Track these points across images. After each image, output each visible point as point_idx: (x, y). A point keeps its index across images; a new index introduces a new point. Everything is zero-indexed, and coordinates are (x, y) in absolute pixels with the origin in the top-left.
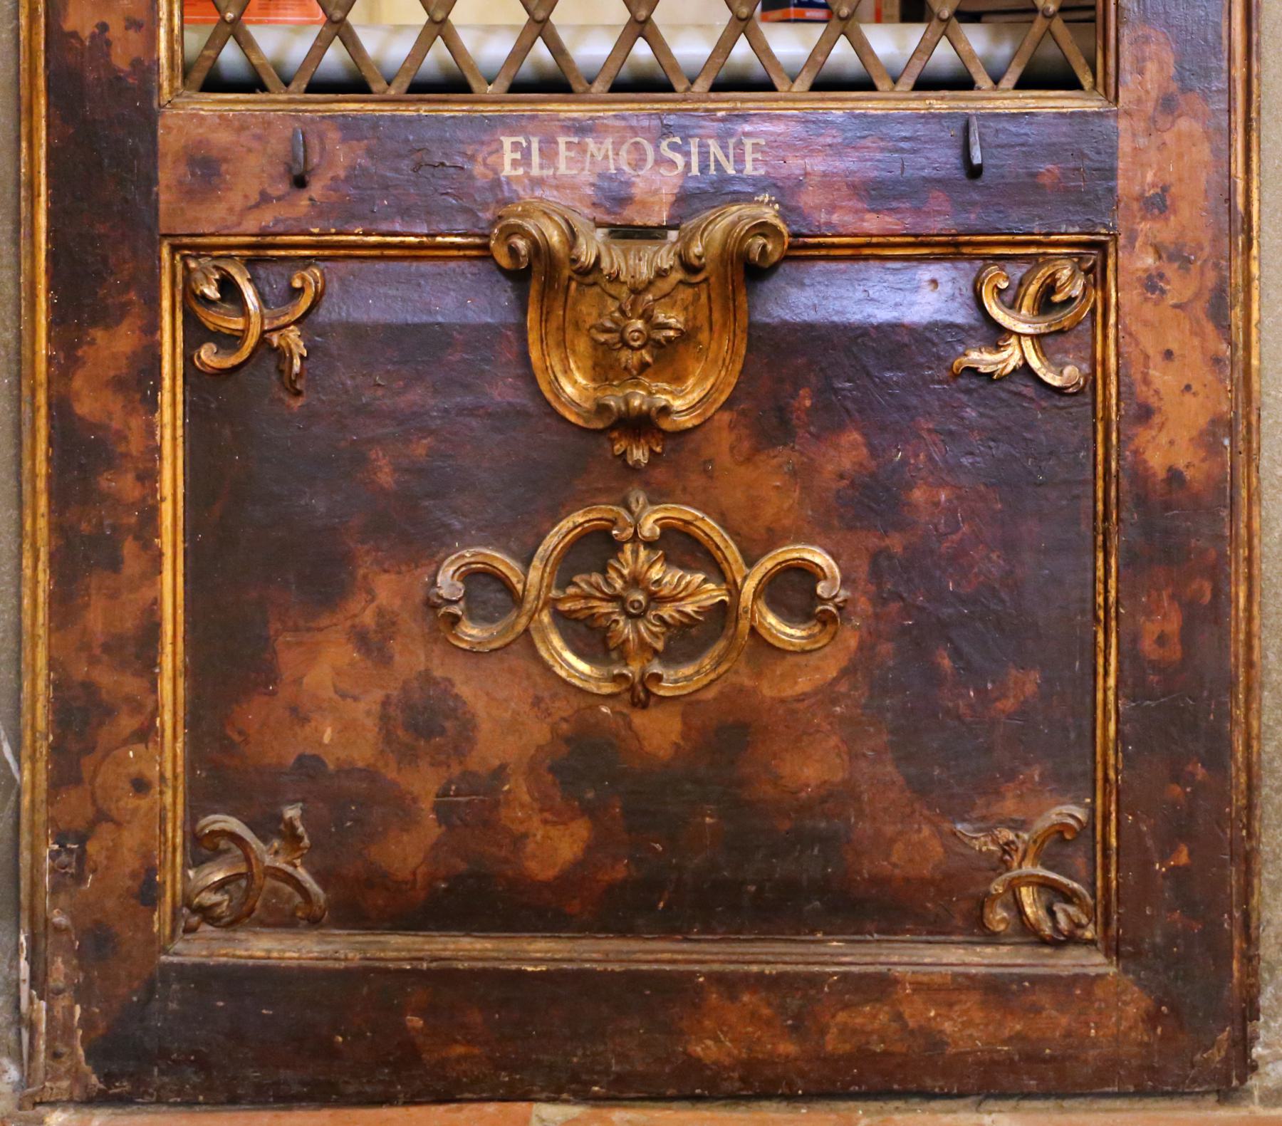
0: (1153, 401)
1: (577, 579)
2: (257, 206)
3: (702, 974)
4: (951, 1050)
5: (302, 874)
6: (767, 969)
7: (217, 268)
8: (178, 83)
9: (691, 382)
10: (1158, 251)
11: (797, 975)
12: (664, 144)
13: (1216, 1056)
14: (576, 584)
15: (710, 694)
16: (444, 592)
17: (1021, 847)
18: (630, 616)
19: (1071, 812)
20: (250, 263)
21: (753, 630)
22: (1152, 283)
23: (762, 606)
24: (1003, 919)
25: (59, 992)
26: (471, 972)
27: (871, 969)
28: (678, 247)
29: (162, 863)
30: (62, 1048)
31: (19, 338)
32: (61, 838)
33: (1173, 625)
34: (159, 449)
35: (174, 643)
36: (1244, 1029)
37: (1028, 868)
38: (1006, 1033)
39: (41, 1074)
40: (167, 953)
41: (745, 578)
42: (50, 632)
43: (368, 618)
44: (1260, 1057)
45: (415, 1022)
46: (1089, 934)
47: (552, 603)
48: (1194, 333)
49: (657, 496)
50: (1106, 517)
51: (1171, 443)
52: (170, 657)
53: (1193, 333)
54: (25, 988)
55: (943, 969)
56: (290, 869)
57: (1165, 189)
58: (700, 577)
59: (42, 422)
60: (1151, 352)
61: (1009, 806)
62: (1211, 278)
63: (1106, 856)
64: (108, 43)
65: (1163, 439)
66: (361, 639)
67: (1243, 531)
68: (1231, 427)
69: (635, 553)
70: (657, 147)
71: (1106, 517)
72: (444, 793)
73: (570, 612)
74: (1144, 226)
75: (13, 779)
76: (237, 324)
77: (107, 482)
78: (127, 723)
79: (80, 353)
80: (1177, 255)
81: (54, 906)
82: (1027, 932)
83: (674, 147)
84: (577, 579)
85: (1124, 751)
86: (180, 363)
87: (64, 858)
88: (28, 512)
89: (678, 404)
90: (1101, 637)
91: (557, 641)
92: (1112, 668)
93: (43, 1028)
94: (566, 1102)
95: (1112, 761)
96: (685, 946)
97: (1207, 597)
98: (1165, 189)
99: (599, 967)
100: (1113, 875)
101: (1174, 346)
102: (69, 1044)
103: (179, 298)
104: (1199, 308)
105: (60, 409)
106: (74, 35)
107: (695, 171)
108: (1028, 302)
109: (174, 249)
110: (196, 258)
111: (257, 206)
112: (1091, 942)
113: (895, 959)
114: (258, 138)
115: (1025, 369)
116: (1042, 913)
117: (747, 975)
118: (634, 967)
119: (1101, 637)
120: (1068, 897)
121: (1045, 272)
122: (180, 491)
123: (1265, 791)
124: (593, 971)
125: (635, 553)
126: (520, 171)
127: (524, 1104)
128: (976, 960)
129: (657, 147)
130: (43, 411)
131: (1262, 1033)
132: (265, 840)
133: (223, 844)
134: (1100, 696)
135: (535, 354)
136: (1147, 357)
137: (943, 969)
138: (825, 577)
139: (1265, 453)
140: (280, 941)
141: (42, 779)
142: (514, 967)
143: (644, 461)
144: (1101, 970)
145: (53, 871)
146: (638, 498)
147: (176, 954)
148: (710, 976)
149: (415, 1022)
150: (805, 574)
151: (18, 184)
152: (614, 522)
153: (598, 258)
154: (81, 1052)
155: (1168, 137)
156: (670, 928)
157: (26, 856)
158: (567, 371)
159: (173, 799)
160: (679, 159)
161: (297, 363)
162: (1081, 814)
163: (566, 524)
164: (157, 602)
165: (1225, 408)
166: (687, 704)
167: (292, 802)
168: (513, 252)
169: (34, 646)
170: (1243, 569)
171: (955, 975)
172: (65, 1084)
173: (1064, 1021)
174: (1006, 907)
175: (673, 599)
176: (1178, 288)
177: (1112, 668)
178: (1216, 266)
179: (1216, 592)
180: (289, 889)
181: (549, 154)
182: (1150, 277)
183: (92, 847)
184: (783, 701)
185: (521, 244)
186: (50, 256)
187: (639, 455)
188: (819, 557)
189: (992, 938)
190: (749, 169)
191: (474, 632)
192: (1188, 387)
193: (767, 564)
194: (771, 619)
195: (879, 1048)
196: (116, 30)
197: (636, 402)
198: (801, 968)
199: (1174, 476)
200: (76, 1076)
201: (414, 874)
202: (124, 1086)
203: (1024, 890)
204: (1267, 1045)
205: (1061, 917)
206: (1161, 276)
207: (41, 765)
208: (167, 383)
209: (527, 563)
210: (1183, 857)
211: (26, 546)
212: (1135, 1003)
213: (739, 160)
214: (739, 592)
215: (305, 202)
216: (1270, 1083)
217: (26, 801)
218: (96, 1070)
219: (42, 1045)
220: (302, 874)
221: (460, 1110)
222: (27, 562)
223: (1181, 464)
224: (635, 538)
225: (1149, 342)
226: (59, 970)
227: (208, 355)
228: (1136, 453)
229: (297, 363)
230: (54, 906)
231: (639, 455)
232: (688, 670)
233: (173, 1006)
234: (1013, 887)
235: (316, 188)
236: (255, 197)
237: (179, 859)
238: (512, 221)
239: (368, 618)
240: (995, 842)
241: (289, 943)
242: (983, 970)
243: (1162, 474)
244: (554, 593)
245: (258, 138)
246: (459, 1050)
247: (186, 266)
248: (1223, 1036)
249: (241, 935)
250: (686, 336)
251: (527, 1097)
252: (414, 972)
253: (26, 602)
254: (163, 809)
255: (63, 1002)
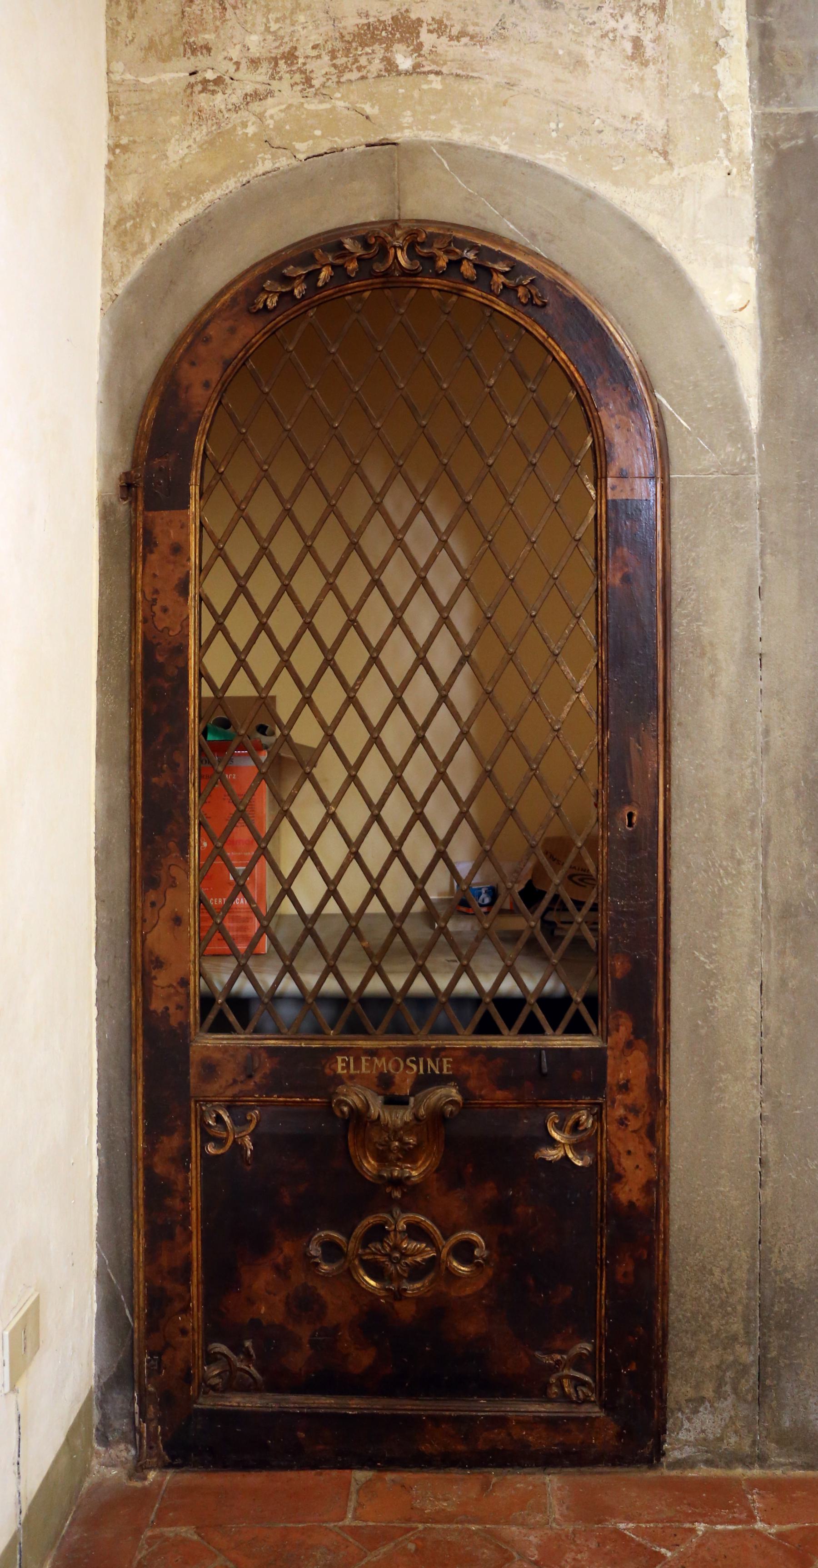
0: (622, 1172)
1: (370, 1246)
2: (232, 1085)
3: (424, 1415)
4: (532, 1449)
5: (253, 1370)
6: (453, 1414)
7: (215, 1111)
8: (198, 1030)
9: (420, 1163)
10: (626, 1107)
11: (466, 1417)
12: (408, 1060)
13: (647, 1451)
14: (370, 1248)
15: (429, 1294)
16: (313, 1253)
17: (563, 1362)
18: (393, 1263)
19: (585, 1347)
20: (229, 1108)
21: (447, 1269)
22: (622, 1122)
23: (451, 1258)
24: (555, 1393)
25: (152, 1420)
26: (325, 1414)
27: (498, 1414)
28: (414, 1110)
29: (194, 1364)
30: (153, 1444)
31: (131, 1136)
32: (151, 1354)
33: (631, 1268)
34: (191, 1188)
35: (197, 1270)
36: (659, 1438)
37: (566, 1372)
38: (556, 1442)
39: (145, 1455)
40: (196, 1403)
41: (443, 1247)
42: (145, 1266)
43: (280, 1260)
44: (667, 1449)
45: (302, 1435)
46: (592, 1399)
47: (360, 1257)
48: (640, 1143)
49: (404, 1210)
50: (602, 1221)
51: (630, 1190)
52: (196, 1276)
53: (640, 1143)
54: (137, 1416)
55: (529, 1414)
56: (247, 1368)
57: (628, 1081)
58: (424, 1245)
59: (141, 1175)
60: (622, 1151)
61: (558, 1344)
62: (648, 1120)
63: (600, 1366)
64: (169, 1016)
65: (627, 1188)
66: (277, 1268)
67: (662, 1229)
68: (657, 1183)
69: (395, 1236)
70: (405, 1062)
71: (602, 1221)
72: (313, 1335)
73: (367, 1260)
74: (619, 1097)
75: (130, 1324)
76: (224, 1135)
77: (169, 1202)
78: (178, 1305)
79: (157, 1147)
80: (633, 1109)
81: (149, 1383)
82: (565, 1398)
83: (412, 1061)
84: (370, 1246)
85: (609, 1321)
86: (199, 1151)
87: (152, 1362)
88: (135, 1212)
89: (414, 1173)
90: (599, 1272)
91: (362, 1272)
92: (604, 1286)
93: (145, 1435)
94: (366, 1470)
95: (603, 1326)
96: (418, 1402)
97: (645, 1257)
98: (628, 1081)
99: (379, 1412)
100: (603, 1374)
101: (632, 1149)
102: (156, 1443)
103: (198, 1123)
104: (643, 1133)
105: (149, 1170)
106: (155, 1012)
107: (422, 1072)
108: (567, 1129)
109: (196, 1102)
110: (205, 1105)
111: (232, 1085)
112: (594, 1402)
113: (508, 1409)
114: (232, 1056)
115: (566, 1157)
116: (572, 1390)
117: (445, 1416)
118: (395, 1412)
119: (599, 1272)
120: (584, 1383)
121: (576, 1116)
122: (199, 1204)
123: (670, 1336)
124: (377, 1414)
125: (395, 1236)
126: (345, 1071)
127: (348, 1471)
128: (543, 1409)
129: (405, 1062)
130: (141, 1171)
131: (667, 1439)
132: (237, 1354)
133: (219, 1356)
134: (598, 1297)
135: (351, 1150)
136: (620, 1154)
137: (529, 1414)
138: (478, 1247)
139: (671, 1191)
140: (244, 1398)
141: (142, 1328)
142: (343, 1412)
143: (399, 1196)
144: (598, 1415)
145: (148, 1368)
146: (397, 1211)
147: (201, 1404)
148: (428, 1417)
149: (302, 1435)
150: (470, 1245)
151: (130, 1071)
152: (386, 1223)
153: (379, 1116)
154: (161, 1446)
155: (629, 1059)
156: (411, 1394)
157: (136, 1360)
158: (366, 1158)
159: (198, 1338)
160: (414, 1067)
161: (249, 1153)
162: (589, 1347)
163: (365, 1222)
164: (190, 1254)
165: (654, 1175)
166: (419, 1300)
167: (248, 1339)
168: (342, 1112)
169: (139, 1271)
170: (662, 1244)
171: (534, 1417)
172: (155, 1460)
173: (581, 1436)
174: (557, 1386)
175: (411, 1255)
176: (634, 1123)
177: (604, 1286)
178: (650, 1114)
179: (649, 1255)
180: (247, 1376)
181: (357, 1061)
182: (621, 1119)
183: (164, 1358)
184: (460, 1298)
185: (345, 1109)
186: (144, 1104)
187: (397, 1194)
188: (475, 1237)
189: (550, 1401)
190: (445, 1071)
191: (326, 1267)
192: (637, 1167)
193: (453, 1240)
194: (455, 1264)
195: (501, 1447)
196: (172, 1010)
197: (396, 1174)
198: (467, 1413)
199: (631, 1204)
200: (159, 1455)
201: (300, 1369)
202: (178, 1461)
203: (564, 1380)
204: (670, 1444)
205: (580, 1393)
206: (626, 1118)
207: (142, 1322)
208: (194, 1159)
209: (348, 1238)
210: (633, 1367)
211: (135, 1226)
212: (612, 1430)
213: (441, 1069)
214: (440, 1253)
215: (252, 1083)
216: (670, 1460)
217: (136, 1336)
218: (168, 1454)
219: (145, 1442)
220: (253, 1370)
221: (321, 1474)
222: (135, 1233)
223: (634, 1199)
224: (395, 1230)
225: (621, 1148)
226: (151, 1410)
227: (211, 1149)
228: (615, 1194)
229: (249, 1153)
230: (149, 1383)
231: (397, 1194)
232: (418, 1285)
233: (199, 1427)
234: (560, 1380)
235: (257, 1078)
236: (231, 1081)
237: (200, 1362)
238: (342, 1098)
239: (280, 1260)
240: (552, 1359)
241: (247, 1399)
242: (546, 1414)
243: (626, 1203)
244: (360, 1251)
245: (232, 1056)
246: (321, 1447)
247: (201, 1109)
248: (650, 1443)
249: (227, 1395)
250: (418, 1146)
251: (350, 1467)
252: (302, 1414)
253: (135, 1250)
254: (194, 1341)
255: (153, 1425)
